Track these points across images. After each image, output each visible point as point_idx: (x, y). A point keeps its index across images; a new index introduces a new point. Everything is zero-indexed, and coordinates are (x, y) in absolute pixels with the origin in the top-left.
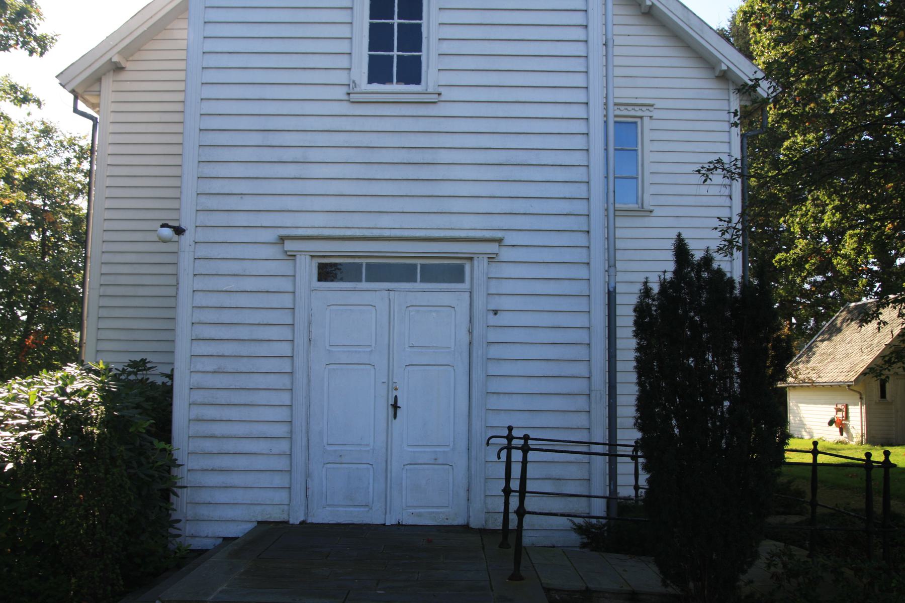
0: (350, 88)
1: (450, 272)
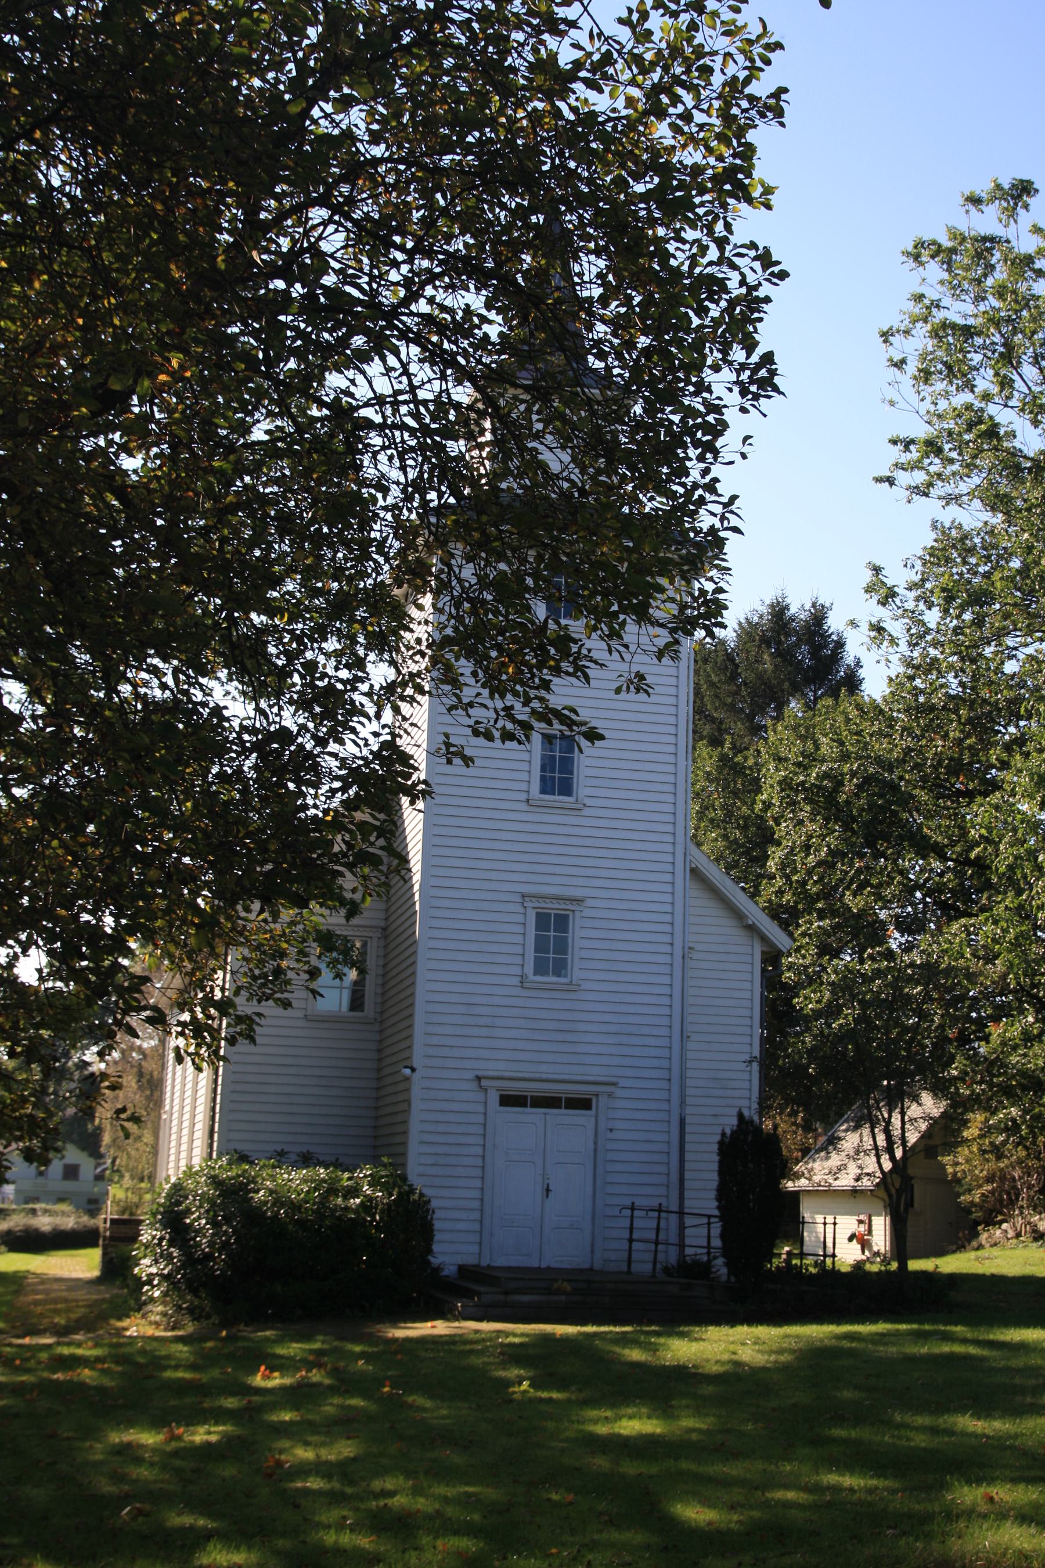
0: (523, 977)
1: (582, 1104)
